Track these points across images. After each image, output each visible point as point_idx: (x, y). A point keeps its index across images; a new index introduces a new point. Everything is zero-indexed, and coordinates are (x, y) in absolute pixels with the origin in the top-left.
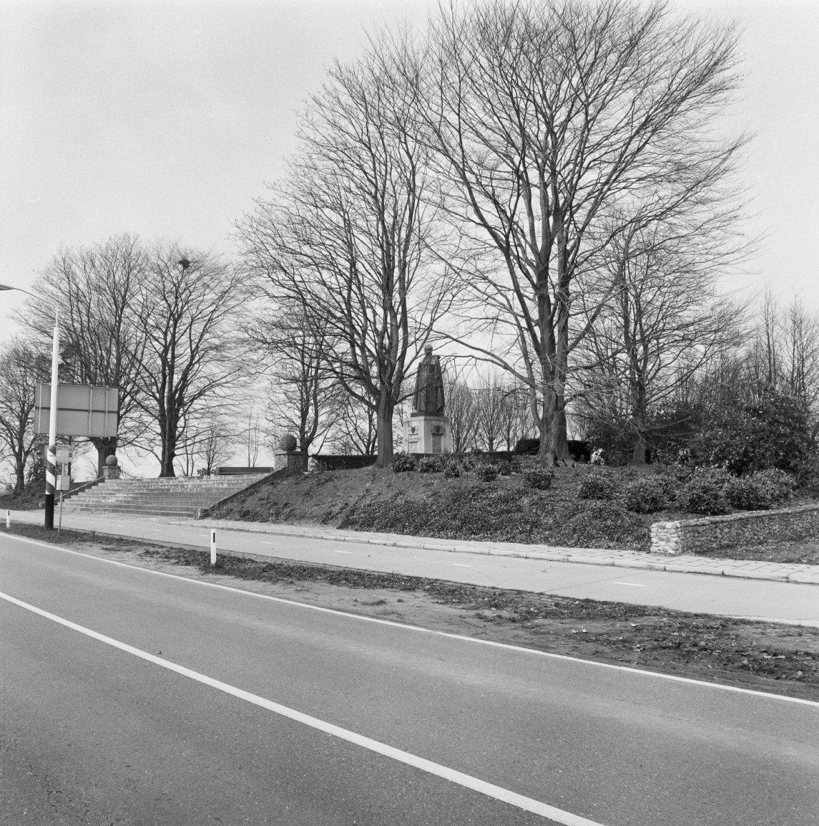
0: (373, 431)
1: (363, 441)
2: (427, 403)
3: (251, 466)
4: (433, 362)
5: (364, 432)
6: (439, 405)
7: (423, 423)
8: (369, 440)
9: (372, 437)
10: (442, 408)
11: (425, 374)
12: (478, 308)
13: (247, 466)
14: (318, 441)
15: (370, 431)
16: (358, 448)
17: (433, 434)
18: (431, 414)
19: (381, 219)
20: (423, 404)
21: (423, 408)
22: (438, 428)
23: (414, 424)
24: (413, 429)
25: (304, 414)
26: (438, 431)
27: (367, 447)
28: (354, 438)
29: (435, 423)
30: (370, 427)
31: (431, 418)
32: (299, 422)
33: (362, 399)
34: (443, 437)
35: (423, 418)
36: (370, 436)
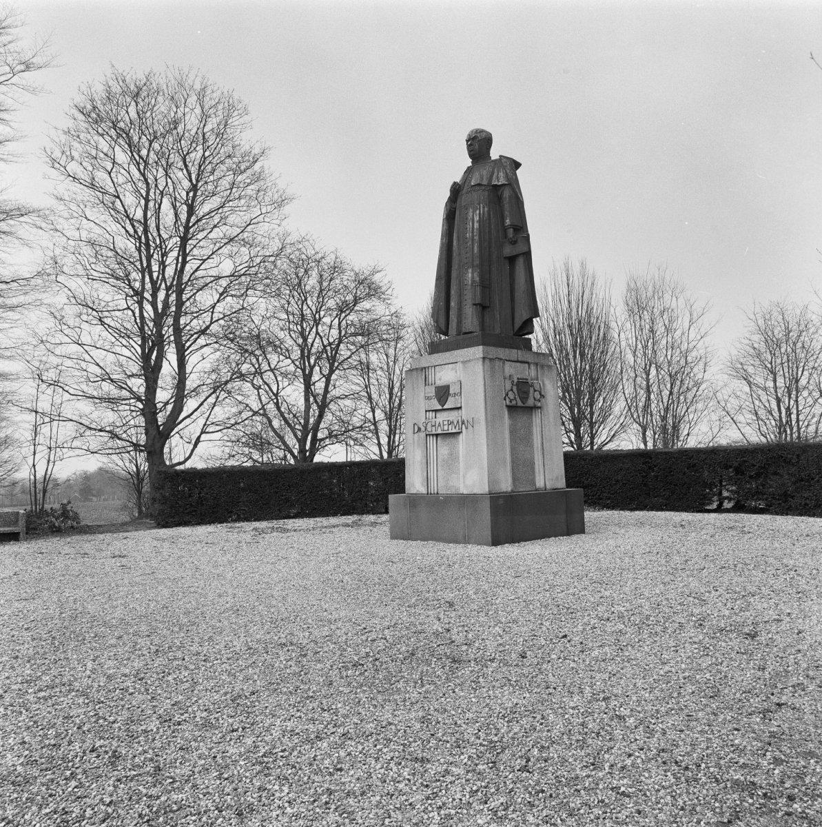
0: (315, 407)
1: (293, 429)
2: (483, 308)
3: (349, 460)
5: (294, 410)
7: (478, 369)
10: (527, 326)
11: (474, 218)
13: (345, 460)
14: (190, 428)
15: (308, 407)
17: (511, 408)
19: (191, 180)
20: (469, 311)
21: (471, 320)
22: (523, 387)
23: (445, 376)
24: (443, 393)
25: (151, 373)
26: (524, 398)
27: (302, 442)
28: (276, 423)
30: (307, 400)
31: (502, 353)
32: (138, 385)
34: (536, 419)
35: (477, 351)
36: (307, 420)
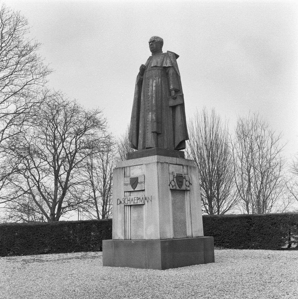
0: (60, 189)
2: (157, 134)
4: (168, 64)
5: (48, 190)
6: (179, 138)
7: (155, 169)
8: (54, 200)
9: (58, 196)
10: (182, 145)
12: (65, 173)
15: (56, 189)
16: (42, 210)
18: (167, 154)
21: (151, 141)
22: (180, 179)
23: (136, 172)
24: (134, 182)
27: (52, 209)
29: (174, 169)
30: (56, 185)
31: (168, 159)
33: (97, 211)
34: (187, 196)
35: (154, 158)
36: (56, 196)
